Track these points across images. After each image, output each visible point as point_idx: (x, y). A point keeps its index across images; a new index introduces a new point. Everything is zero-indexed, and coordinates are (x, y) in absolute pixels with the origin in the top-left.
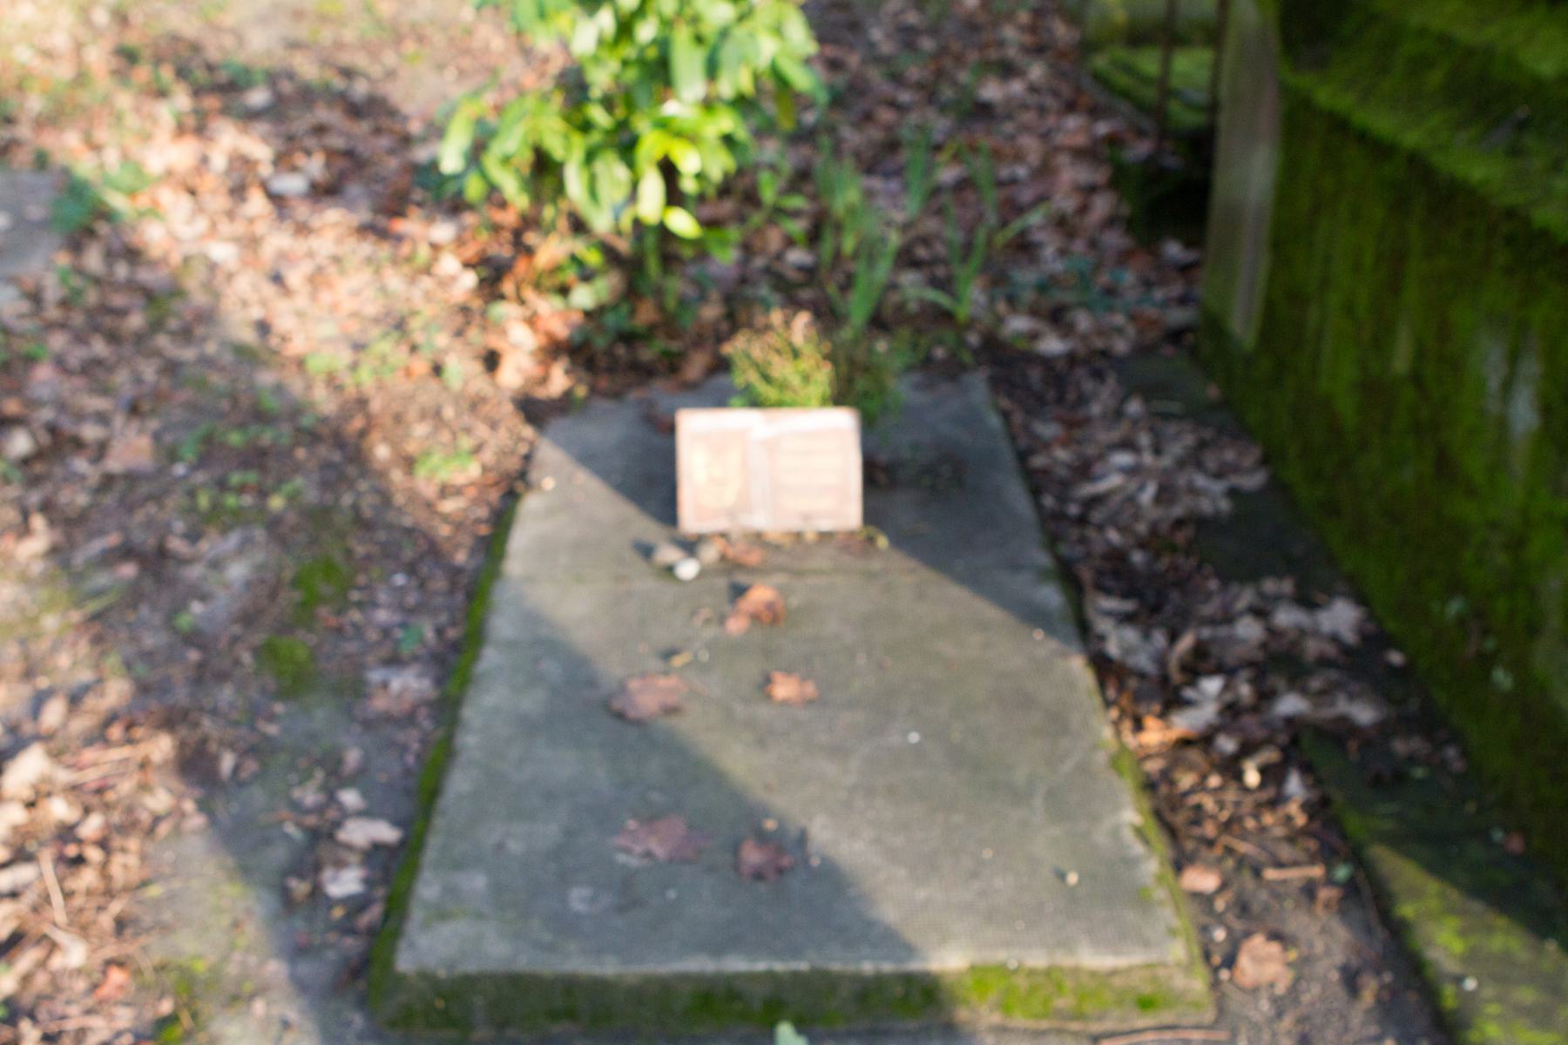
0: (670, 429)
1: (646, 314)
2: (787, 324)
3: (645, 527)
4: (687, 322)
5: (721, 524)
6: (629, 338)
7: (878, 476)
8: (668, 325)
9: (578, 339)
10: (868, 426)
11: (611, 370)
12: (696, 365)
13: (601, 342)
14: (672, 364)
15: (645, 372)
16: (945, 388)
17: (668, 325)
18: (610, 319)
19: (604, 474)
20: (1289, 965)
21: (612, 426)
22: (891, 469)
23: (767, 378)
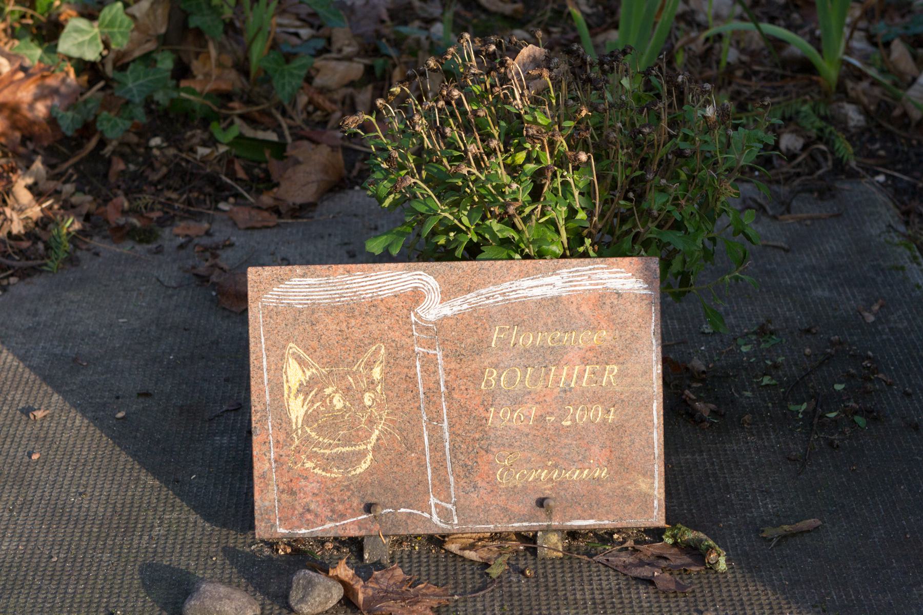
0: (234, 302)
1: (211, 73)
2: (494, 63)
3: (177, 529)
4: (286, 85)
5: (351, 525)
6: (171, 120)
7: (693, 397)
8: (252, 95)
9: (69, 123)
10: (675, 292)
11: (134, 185)
12: (301, 180)
13: (114, 128)
14: (258, 172)
15: (205, 188)
16: (808, 208)
17: (252, 95)
18: (133, 84)
19: (96, 410)
20: (101, 54)
21: (122, 299)
22: (713, 382)
23: (445, 188)
